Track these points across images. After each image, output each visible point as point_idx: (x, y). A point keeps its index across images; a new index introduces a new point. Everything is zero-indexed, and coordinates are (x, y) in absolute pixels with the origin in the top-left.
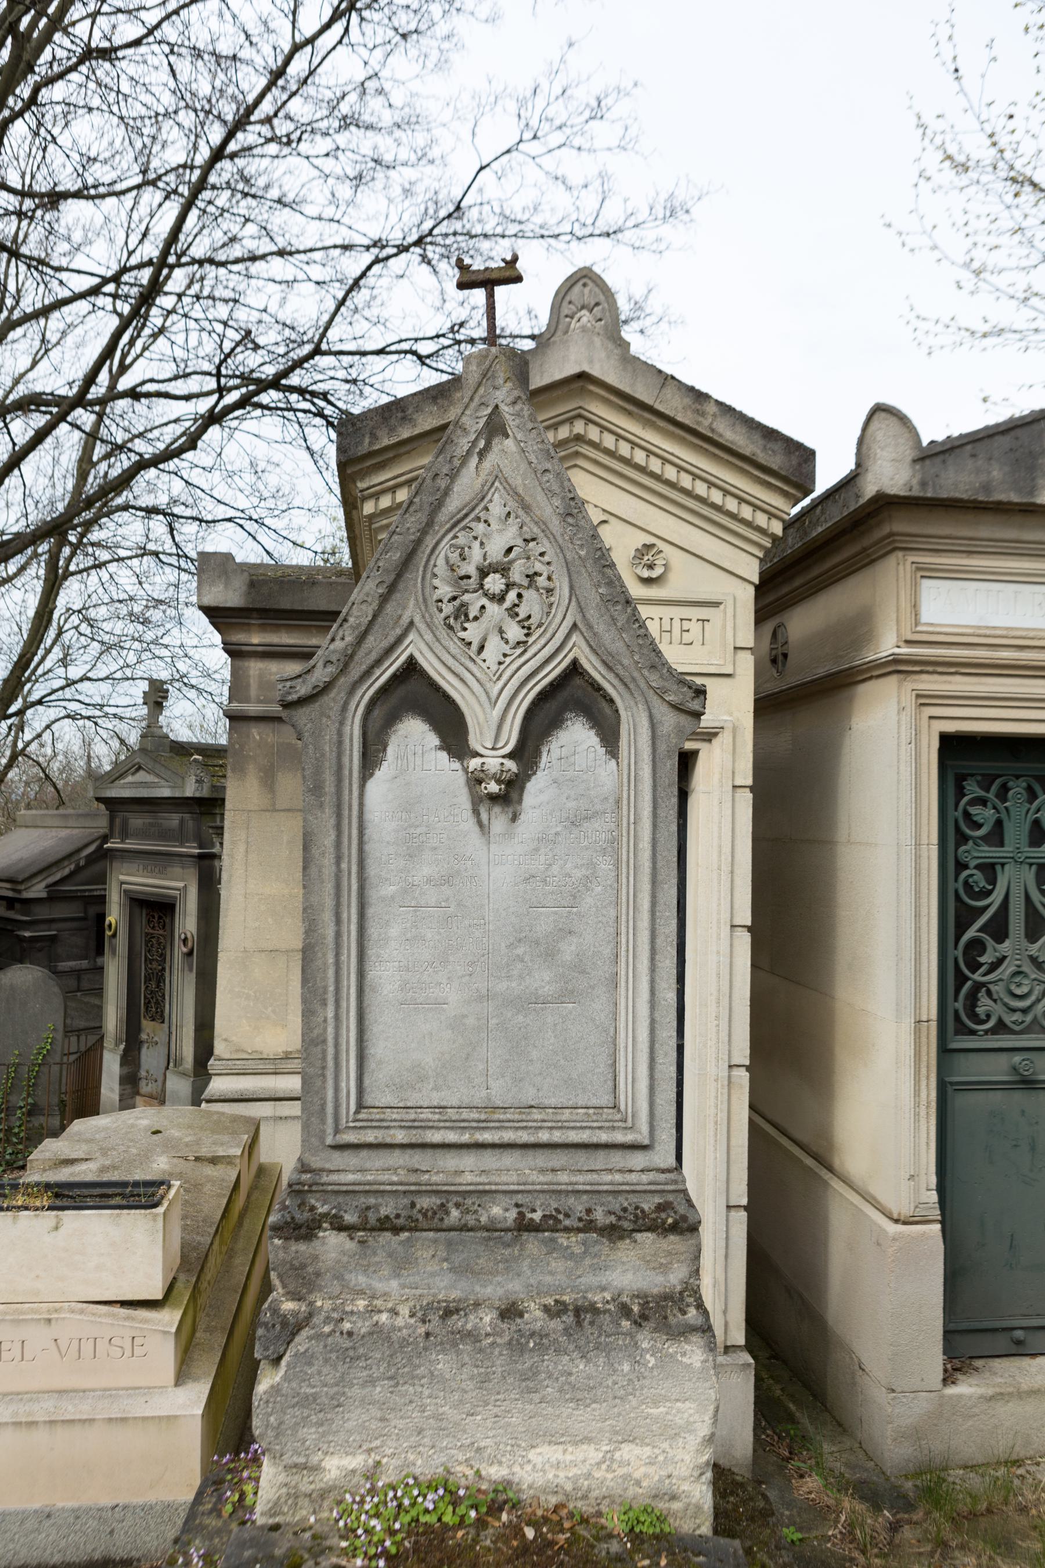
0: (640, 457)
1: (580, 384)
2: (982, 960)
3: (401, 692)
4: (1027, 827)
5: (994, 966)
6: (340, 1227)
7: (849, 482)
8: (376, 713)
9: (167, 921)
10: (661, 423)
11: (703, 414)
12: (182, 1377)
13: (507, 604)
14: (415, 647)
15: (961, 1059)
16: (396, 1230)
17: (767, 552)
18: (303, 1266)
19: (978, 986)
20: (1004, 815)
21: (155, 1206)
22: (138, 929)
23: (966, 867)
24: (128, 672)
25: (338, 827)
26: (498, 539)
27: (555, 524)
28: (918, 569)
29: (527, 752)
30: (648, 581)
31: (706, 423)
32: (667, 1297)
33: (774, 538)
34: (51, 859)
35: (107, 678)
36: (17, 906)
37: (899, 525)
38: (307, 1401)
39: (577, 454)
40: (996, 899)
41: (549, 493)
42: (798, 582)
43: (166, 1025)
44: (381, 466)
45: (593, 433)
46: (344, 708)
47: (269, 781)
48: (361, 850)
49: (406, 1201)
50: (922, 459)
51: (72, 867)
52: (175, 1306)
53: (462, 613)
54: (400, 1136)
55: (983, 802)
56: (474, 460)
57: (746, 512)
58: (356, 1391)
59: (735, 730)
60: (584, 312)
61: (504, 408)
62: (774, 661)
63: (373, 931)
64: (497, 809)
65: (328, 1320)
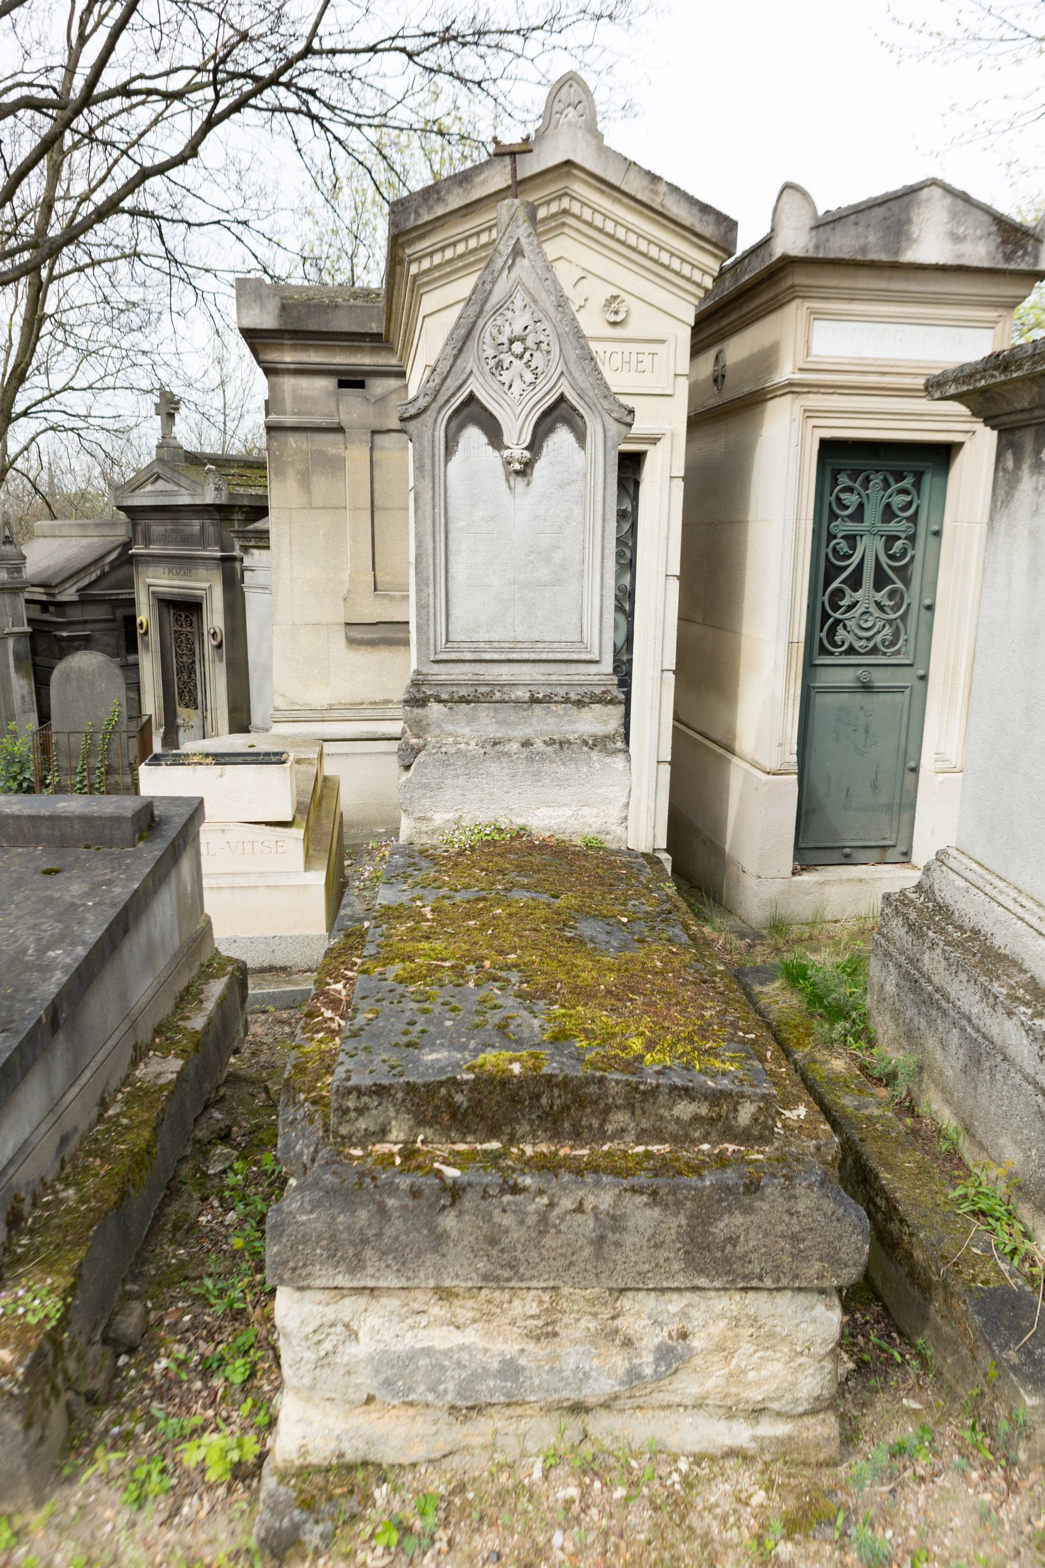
0: (609, 227)
1: (565, 169)
2: (841, 603)
3: (466, 411)
4: (881, 508)
5: (850, 608)
6: (440, 701)
7: (765, 243)
8: (453, 424)
9: (194, 619)
10: (626, 200)
11: (656, 193)
12: (309, 862)
13: (525, 360)
14: (474, 386)
15: (821, 671)
16: (468, 702)
17: (702, 301)
18: (421, 721)
19: (838, 622)
20: (865, 500)
21: (283, 763)
22: (167, 628)
23: (835, 537)
24: (109, 381)
25: (433, 488)
26: (518, 321)
27: (552, 312)
28: (812, 313)
29: (535, 446)
30: (614, 324)
31: (659, 200)
32: (606, 737)
33: (706, 290)
34: (79, 565)
35: (90, 387)
36: (52, 609)
37: (799, 278)
38: (425, 786)
39: (564, 224)
40: (855, 560)
41: (549, 293)
42: (734, 316)
43: (200, 711)
44: (422, 237)
45: (576, 208)
46: (435, 421)
47: (305, 481)
48: (446, 502)
49: (472, 689)
50: (817, 227)
51: (98, 572)
52: (299, 827)
53: (499, 365)
54: (469, 656)
55: (850, 490)
56: (506, 272)
57: (686, 270)
58: (449, 781)
59: (673, 435)
60: (571, 109)
61: (523, 240)
62: (715, 381)
63: (452, 546)
64: (519, 479)
65: (434, 747)
